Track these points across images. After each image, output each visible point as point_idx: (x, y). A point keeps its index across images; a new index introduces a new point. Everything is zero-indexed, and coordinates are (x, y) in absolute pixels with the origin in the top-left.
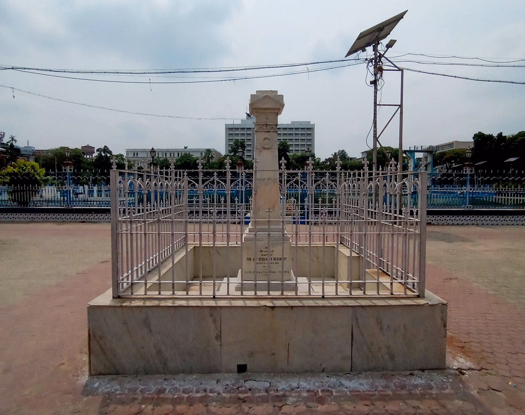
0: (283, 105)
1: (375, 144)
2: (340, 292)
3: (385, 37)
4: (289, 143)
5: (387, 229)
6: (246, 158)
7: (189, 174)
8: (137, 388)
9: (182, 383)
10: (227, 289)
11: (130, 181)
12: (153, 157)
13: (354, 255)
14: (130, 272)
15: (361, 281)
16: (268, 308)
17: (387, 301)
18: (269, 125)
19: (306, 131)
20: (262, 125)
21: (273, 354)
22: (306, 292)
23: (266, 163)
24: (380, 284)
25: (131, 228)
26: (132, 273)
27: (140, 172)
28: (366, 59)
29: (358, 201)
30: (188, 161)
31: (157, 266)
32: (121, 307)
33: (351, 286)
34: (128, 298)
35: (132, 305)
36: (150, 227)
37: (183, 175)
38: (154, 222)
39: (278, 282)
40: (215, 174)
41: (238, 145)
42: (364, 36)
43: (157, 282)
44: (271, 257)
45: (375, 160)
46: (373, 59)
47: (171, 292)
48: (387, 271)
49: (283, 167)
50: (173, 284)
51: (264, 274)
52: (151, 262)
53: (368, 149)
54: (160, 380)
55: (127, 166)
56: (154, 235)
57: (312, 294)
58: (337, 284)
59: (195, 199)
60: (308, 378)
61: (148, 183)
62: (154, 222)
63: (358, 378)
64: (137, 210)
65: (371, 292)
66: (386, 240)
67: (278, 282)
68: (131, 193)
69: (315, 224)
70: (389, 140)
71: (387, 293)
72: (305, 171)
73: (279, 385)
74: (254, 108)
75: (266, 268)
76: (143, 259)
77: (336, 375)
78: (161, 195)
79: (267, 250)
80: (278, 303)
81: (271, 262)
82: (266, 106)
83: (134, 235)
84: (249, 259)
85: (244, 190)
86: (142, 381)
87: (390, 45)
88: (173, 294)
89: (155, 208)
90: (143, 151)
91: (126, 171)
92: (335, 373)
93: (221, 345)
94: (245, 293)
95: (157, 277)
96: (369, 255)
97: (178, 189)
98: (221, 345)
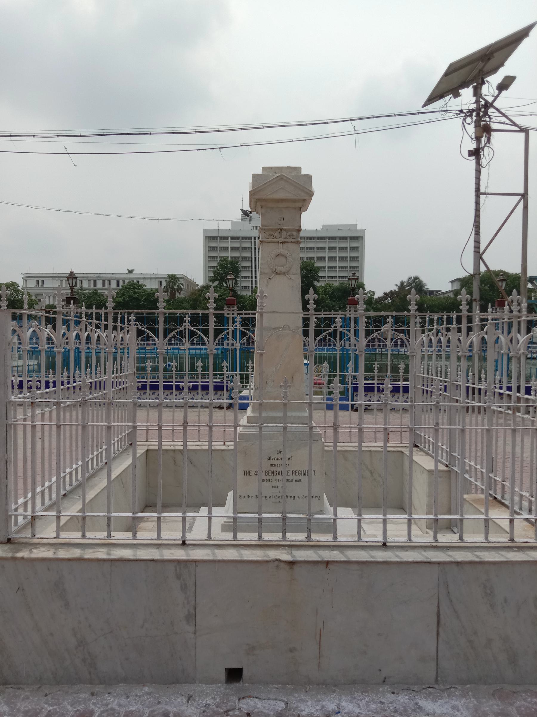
0: (310, 194)
1: (477, 266)
2: (416, 536)
3: (494, 70)
4: (318, 265)
5: (501, 421)
6: (241, 292)
7: (140, 319)
8: (40, 710)
9: (123, 701)
10: (205, 530)
11: (31, 330)
12: (72, 288)
13: (442, 467)
14: (30, 495)
15: (455, 517)
16: (282, 565)
17: (503, 553)
18: (286, 230)
19: (349, 243)
20: (272, 230)
21: (291, 650)
22: (352, 536)
23: (279, 302)
24: (490, 523)
25: (33, 416)
26: (33, 498)
27: (49, 313)
28: (461, 111)
29: (446, 369)
30: (136, 296)
31: (79, 486)
32: (14, 559)
33: (436, 526)
34: (26, 543)
35: (33, 556)
36: (68, 414)
37: (129, 321)
38: (74, 405)
39: (301, 516)
40: (187, 319)
41: (226, 268)
42: (455, 70)
43: (80, 514)
44: (287, 469)
45: (476, 294)
46: (473, 110)
47: (105, 534)
48: (503, 497)
49: (312, 306)
50: (109, 519)
51: (273, 500)
52: (68, 479)
53: (463, 274)
54: (83, 696)
55: (26, 302)
56: (74, 427)
57: (364, 539)
58: (409, 520)
59: (149, 364)
60: (357, 695)
61: (115, 337)
62: (74, 406)
63: (449, 696)
64: (43, 385)
65: (474, 538)
66: (501, 440)
67: (301, 516)
68: (34, 352)
69: (366, 410)
70: (503, 258)
71: (504, 539)
72: (348, 314)
73: (302, 706)
74: (259, 200)
75: (280, 489)
76: (54, 471)
77: (408, 689)
78: (88, 358)
79: (280, 456)
80: (301, 555)
81: (288, 478)
82: (280, 195)
83: (38, 428)
84: (248, 473)
85: (237, 346)
86: (49, 698)
87: (504, 86)
88: (109, 536)
89: (77, 379)
90: (54, 277)
91: (26, 311)
92: (406, 687)
93: (195, 633)
94: (240, 535)
95: (79, 506)
96: (467, 468)
97: (119, 345)
98: (195, 633)
